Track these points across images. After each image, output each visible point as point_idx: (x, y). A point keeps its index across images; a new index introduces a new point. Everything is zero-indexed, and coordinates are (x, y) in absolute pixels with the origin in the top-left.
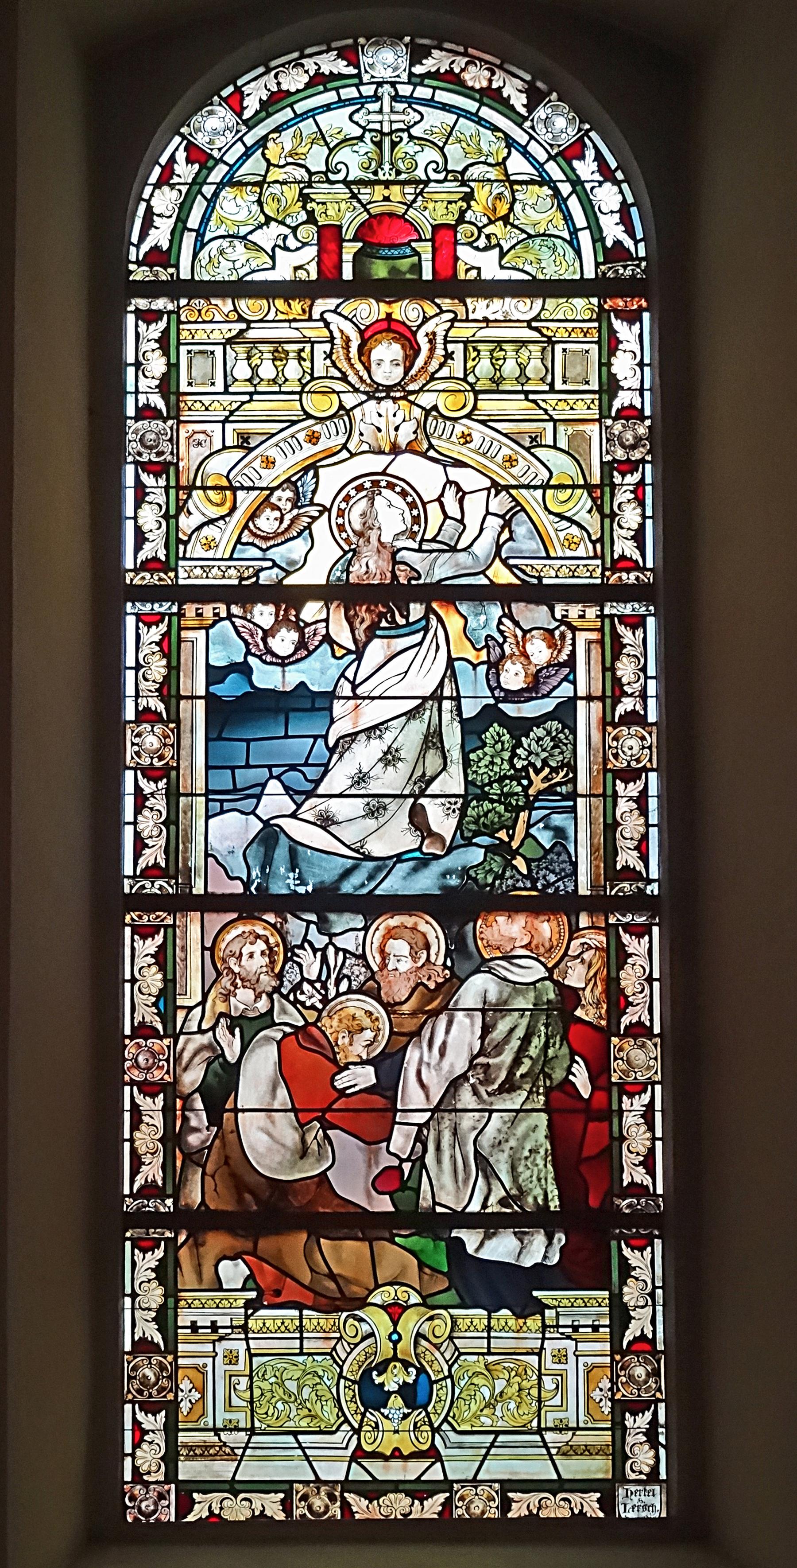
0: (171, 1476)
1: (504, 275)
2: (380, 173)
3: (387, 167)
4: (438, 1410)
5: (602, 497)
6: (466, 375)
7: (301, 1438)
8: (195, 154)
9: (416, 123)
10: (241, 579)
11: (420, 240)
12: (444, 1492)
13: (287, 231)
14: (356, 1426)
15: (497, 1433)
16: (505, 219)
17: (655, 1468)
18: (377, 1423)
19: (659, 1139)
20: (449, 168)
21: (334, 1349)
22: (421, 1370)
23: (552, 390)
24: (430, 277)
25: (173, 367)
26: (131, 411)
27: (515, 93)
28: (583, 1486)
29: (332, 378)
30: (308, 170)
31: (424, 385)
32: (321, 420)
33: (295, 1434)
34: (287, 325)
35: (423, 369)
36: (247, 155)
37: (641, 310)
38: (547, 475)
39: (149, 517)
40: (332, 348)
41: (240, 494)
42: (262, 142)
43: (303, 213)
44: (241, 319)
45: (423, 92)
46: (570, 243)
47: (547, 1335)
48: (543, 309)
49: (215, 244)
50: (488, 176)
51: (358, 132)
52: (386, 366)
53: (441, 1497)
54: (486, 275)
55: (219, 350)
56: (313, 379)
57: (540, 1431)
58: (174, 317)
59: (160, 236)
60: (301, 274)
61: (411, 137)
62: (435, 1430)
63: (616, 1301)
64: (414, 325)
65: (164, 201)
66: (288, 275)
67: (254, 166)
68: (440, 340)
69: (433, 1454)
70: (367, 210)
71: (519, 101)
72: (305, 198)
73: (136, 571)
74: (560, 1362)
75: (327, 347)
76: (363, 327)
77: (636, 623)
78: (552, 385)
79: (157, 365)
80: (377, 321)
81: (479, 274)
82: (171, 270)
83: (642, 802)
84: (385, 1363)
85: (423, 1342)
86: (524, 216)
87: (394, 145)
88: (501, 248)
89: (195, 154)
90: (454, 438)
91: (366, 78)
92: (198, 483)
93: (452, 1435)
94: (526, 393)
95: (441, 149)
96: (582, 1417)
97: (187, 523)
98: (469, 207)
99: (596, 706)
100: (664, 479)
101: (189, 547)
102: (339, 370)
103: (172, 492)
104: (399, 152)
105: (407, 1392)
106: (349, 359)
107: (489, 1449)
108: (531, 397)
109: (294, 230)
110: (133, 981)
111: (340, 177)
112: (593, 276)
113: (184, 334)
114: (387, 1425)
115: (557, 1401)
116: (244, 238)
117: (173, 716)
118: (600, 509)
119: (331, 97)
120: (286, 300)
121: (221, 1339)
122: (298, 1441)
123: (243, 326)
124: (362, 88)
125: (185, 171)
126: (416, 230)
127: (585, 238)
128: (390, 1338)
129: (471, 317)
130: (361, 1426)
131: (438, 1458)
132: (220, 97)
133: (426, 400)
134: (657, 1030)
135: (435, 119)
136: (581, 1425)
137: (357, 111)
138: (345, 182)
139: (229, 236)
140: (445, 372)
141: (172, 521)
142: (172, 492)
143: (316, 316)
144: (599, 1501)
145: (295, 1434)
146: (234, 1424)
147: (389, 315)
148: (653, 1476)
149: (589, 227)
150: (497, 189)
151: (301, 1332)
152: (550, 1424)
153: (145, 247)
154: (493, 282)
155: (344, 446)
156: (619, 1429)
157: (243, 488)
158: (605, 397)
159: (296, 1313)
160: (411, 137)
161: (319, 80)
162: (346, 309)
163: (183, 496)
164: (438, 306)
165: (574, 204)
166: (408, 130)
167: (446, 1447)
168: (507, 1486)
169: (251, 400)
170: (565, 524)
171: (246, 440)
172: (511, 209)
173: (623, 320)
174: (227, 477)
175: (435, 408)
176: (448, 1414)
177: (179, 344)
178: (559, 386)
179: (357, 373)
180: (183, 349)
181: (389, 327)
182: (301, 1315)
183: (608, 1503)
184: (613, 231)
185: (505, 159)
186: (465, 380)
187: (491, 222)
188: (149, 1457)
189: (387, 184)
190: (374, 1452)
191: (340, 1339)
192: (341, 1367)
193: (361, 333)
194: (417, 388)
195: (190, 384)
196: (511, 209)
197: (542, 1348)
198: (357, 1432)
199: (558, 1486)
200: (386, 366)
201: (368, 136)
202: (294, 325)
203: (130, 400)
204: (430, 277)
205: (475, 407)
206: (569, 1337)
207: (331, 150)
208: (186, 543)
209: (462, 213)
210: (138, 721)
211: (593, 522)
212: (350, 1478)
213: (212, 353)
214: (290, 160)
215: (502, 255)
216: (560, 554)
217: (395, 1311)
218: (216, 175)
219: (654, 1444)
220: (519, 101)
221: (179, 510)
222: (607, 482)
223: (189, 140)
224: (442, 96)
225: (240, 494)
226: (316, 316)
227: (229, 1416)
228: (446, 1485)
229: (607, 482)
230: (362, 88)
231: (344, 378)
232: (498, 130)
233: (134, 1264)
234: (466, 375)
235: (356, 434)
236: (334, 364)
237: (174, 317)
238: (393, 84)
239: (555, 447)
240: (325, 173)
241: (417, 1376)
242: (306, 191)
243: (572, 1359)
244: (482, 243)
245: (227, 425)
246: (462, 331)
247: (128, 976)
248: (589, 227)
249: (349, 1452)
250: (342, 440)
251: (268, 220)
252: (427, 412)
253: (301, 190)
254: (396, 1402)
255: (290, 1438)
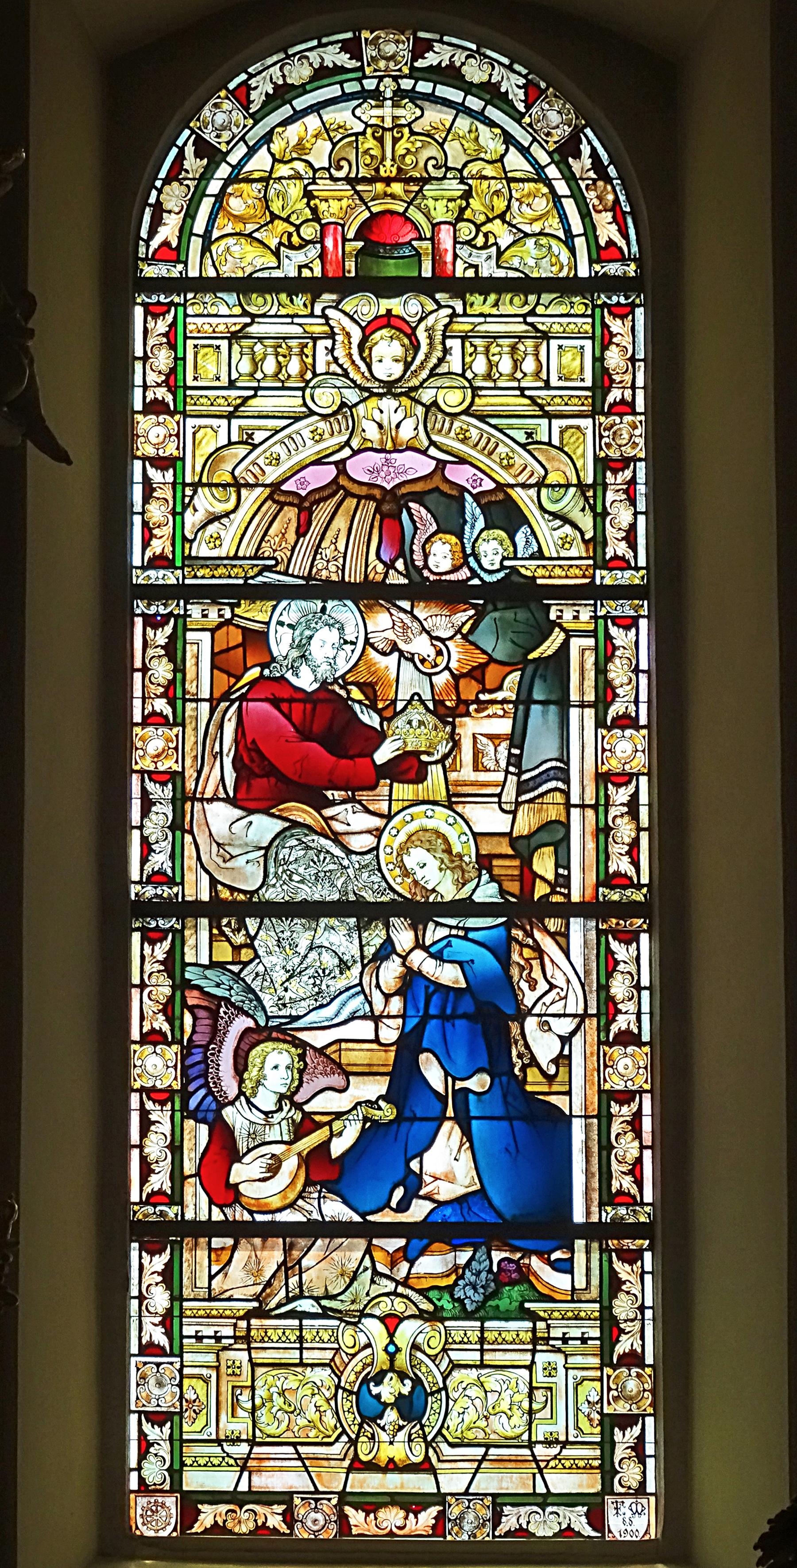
0: (176, 1486)
1: (501, 273)
2: (382, 169)
3: (388, 163)
4: (432, 1419)
5: (595, 497)
6: (464, 371)
7: (302, 1449)
8: (203, 148)
9: (417, 119)
10: (246, 578)
11: (420, 238)
12: (435, 1504)
13: (292, 229)
14: (353, 1436)
15: (488, 1447)
16: (502, 216)
17: (643, 1483)
18: (373, 1435)
19: (645, 829)
20: (449, 164)
21: (333, 1360)
22: (417, 1382)
23: (547, 386)
24: (429, 275)
25: (179, 360)
26: (138, 406)
27: (512, 85)
28: (570, 1500)
29: (334, 374)
30: (311, 165)
31: (425, 381)
32: (324, 417)
33: (294, 1445)
34: (289, 320)
35: (422, 366)
36: (252, 151)
37: (633, 306)
38: (543, 472)
39: (157, 512)
40: (334, 344)
41: (244, 492)
42: (268, 138)
43: (307, 211)
44: (245, 313)
45: (424, 87)
46: (565, 243)
47: (539, 1348)
48: (538, 304)
49: (223, 242)
50: (484, 173)
51: (360, 127)
52: (388, 361)
53: (434, 1511)
54: (485, 273)
55: (224, 344)
56: (315, 375)
57: (530, 1445)
58: (181, 310)
59: (169, 231)
60: (306, 273)
61: (412, 133)
62: (428, 1445)
63: (606, 1313)
64: (413, 321)
65: (174, 197)
66: (293, 273)
67: (261, 161)
68: (438, 337)
69: (425, 1467)
70: (368, 208)
71: (518, 96)
72: (308, 195)
73: (143, 568)
74: (550, 1375)
75: (329, 343)
76: (364, 324)
77: (630, 624)
78: (547, 382)
79: (163, 359)
80: (376, 318)
81: (477, 272)
82: (180, 267)
83: (640, 1448)
84: (382, 1374)
85: (419, 1355)
86: (521, 216)
87: (395, 141)
88: (498, 248)
89: (203, 148)
90: (452, 434)
91: (368, 70)
92: (204, 480)
93: (444, 1447)
94: (522, 390)
95: (441, 145)
96: (572, 1432)
97: (191, 520)
98: (468, 204)
99: (589, 713)
100: (658, 1111)
101: (195, 545)
102: (341, 366)
103: (179, 488)
104: (400, 149)
105: (403, 1405)
106: (350, 355)
107: (480, 1462)
108: (527, 393)
109: (298, 228)
110: (142, 986)
111: (342, 174)
112: (587, 275)
113: (190, 327)
114: (383, 1436)
115: (546, 1413)
116: (250, 235)
117: (179, 720)
118: (593, 508)
119: (335, 91)
120: (289, 295)
121: (225, 1348)
122: (297, 1452)
123: (248, 320)
124: (365, 82)
125: (193, 164)
126: (417, 228)
127: (580, 243)
128: (386, 1350)
129: (469, 311)
130: (358, 1436)
131: (433, 1471)
132: (227, 89)
133: (427, 396)
134: (646, 1038)
135: (435, 116)
136: (571, 1439)
137: (359, 105)
138: (347, 179)
139: (236, 234)
140: (443, 369)
141: (178, 518)
142: (179, 488)
143: (318, 311)
144: (587, 1515)
145: (294, 1445)
146: (236, 1434)
147: (389, 311)
148: (641, 1490)
149: (585, 234)
150: (496, 185)
151: (301, 1343)
152: (541, 1438)
153: (155, 244)
154: (491, 278)
155: (347, 443)
156: (607, 1445)
157: (247, 485)
158: (599, 393)
159: (296, 1322)
160: (412, 133)
161: (322, 74)
162: (348, 305)
163: (188, 491)
164: (437, 302)
165: (569, 205)
166: (409, 125)
167: (439, 1460)
168: (498, 1503)
169: (255, 396)
170: (558, 523)
171: (250, 436)
172: (508, 207)
173: (619, 626)
174: (232, 473)
175: (435, 403)
176: (442, 1426)
177: (186, 338)
178: (554, 382)
179: (358, 368)
180: (190, 343)
181: (388, 320)
182: (301, 1325)
183: (597, 1518)
184: (607, 231)
185: (503, 156)
186: (463, 375)
187: (489, 220)
188: (154, 1471)
189: (388, 181)
190: (370, 1462)
191: (337, 1350)
192: (339, 1378)
193: (363, 329)
194: (417, 383)
195: (195, 379)
196: (508, 207)
197: (533, 1362)
198: (353, 1442)
199: (545, 1500)
200: (388, 361)
201: (369, 131)
202: (296, 320)
203: (138, 393)
204: (429, 275)
205: (472, 403)
206: (559, 1350)
207: (334, 145)
208: (191, 542)
209: (462, 210)
210: (145, 723)
211: (586, 522)
212: (348, 1490)
213: (218, 347)
214: (295, 155)
215: (500, 254)
216: (555, 555)
217: (391, 1322)
218: (224, 171)
219: (641, 1458)
220: (518, 96)
221: (185, 507)
222: (599, 480)
223: (197, 135)
224: (442, 91)
225: (244, 492)
226: (318, 311)
227: (231, 1427)
228: (440, 1498)
229: (599, 480)
230: (365, 82)
231: (346, 374)
232: (498, 126)
233: (141, 1267)
234: (464, 371)
235: (358, 430)
236: (336, 360)
237: (181, 310)
238: (395, 79)
239: (549, 444)
240: (328, 169)
241: (413, 1388)
242: (310, 188)
243: (561, 1371)
244: (480, 241)
245: (233, 421)
246: (462, 325)
247: (136, 980)
248: (585, 234)
249: (346, 1463)
250: (344, 438)
251: (274, 217)
252: (428, 408)
253: (306, 187)
254: (391, 1416)
255: (291, 1449)
